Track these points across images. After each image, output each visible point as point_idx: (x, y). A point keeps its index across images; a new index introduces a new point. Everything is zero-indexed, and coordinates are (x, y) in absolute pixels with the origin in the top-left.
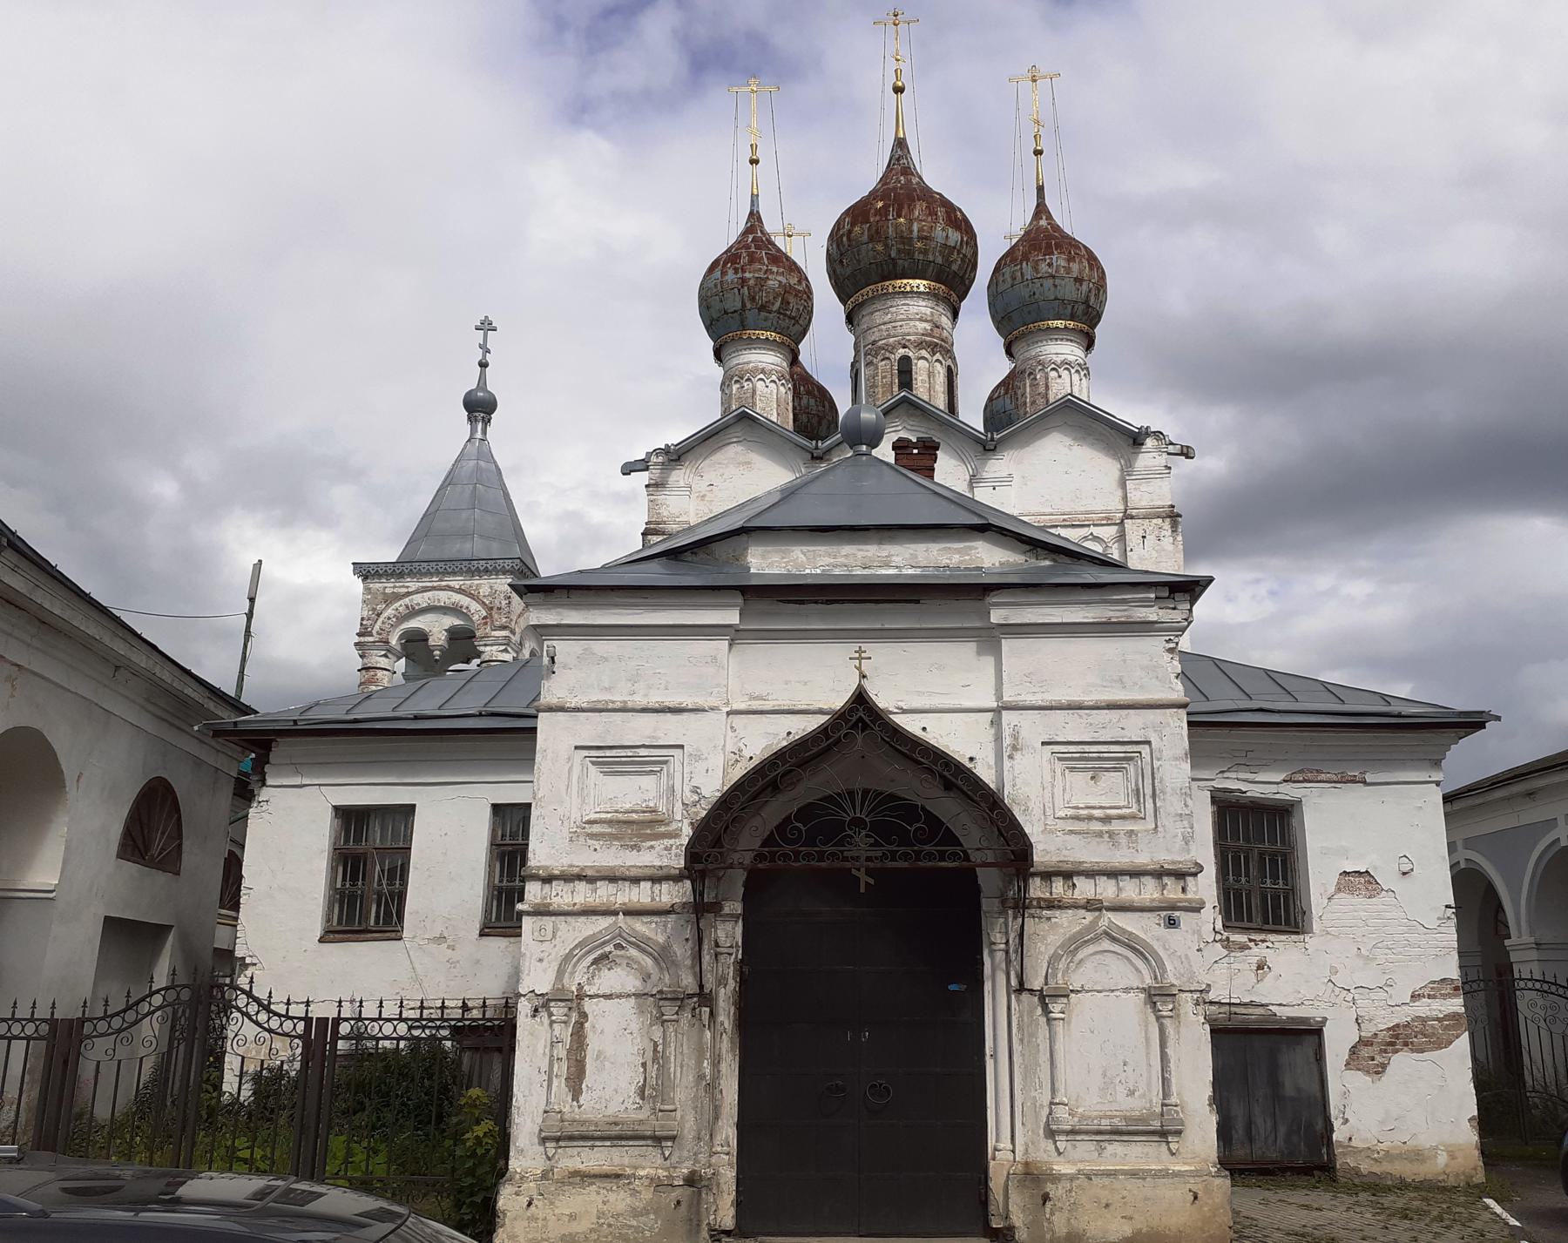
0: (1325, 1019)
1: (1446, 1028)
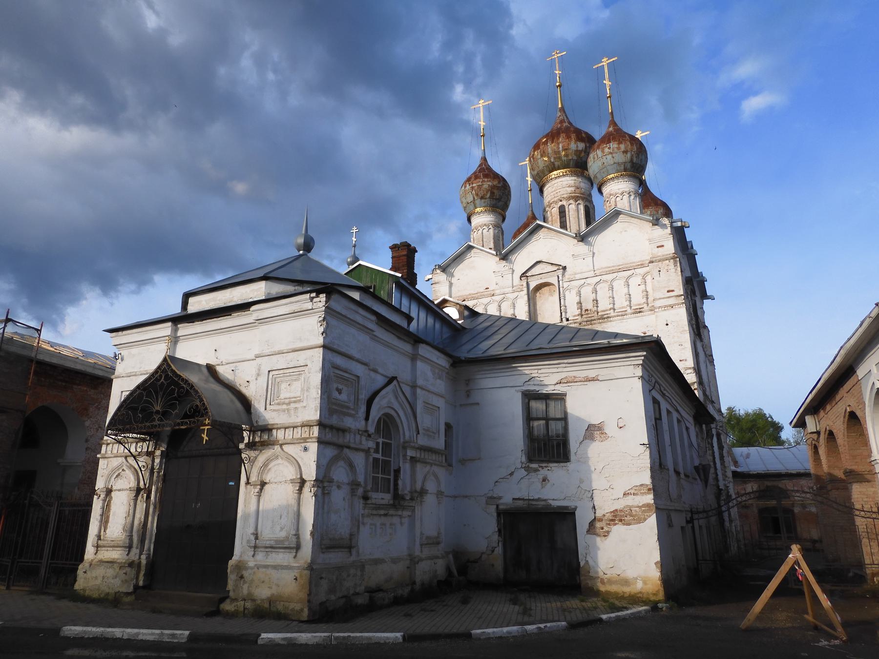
0: (576, 508)
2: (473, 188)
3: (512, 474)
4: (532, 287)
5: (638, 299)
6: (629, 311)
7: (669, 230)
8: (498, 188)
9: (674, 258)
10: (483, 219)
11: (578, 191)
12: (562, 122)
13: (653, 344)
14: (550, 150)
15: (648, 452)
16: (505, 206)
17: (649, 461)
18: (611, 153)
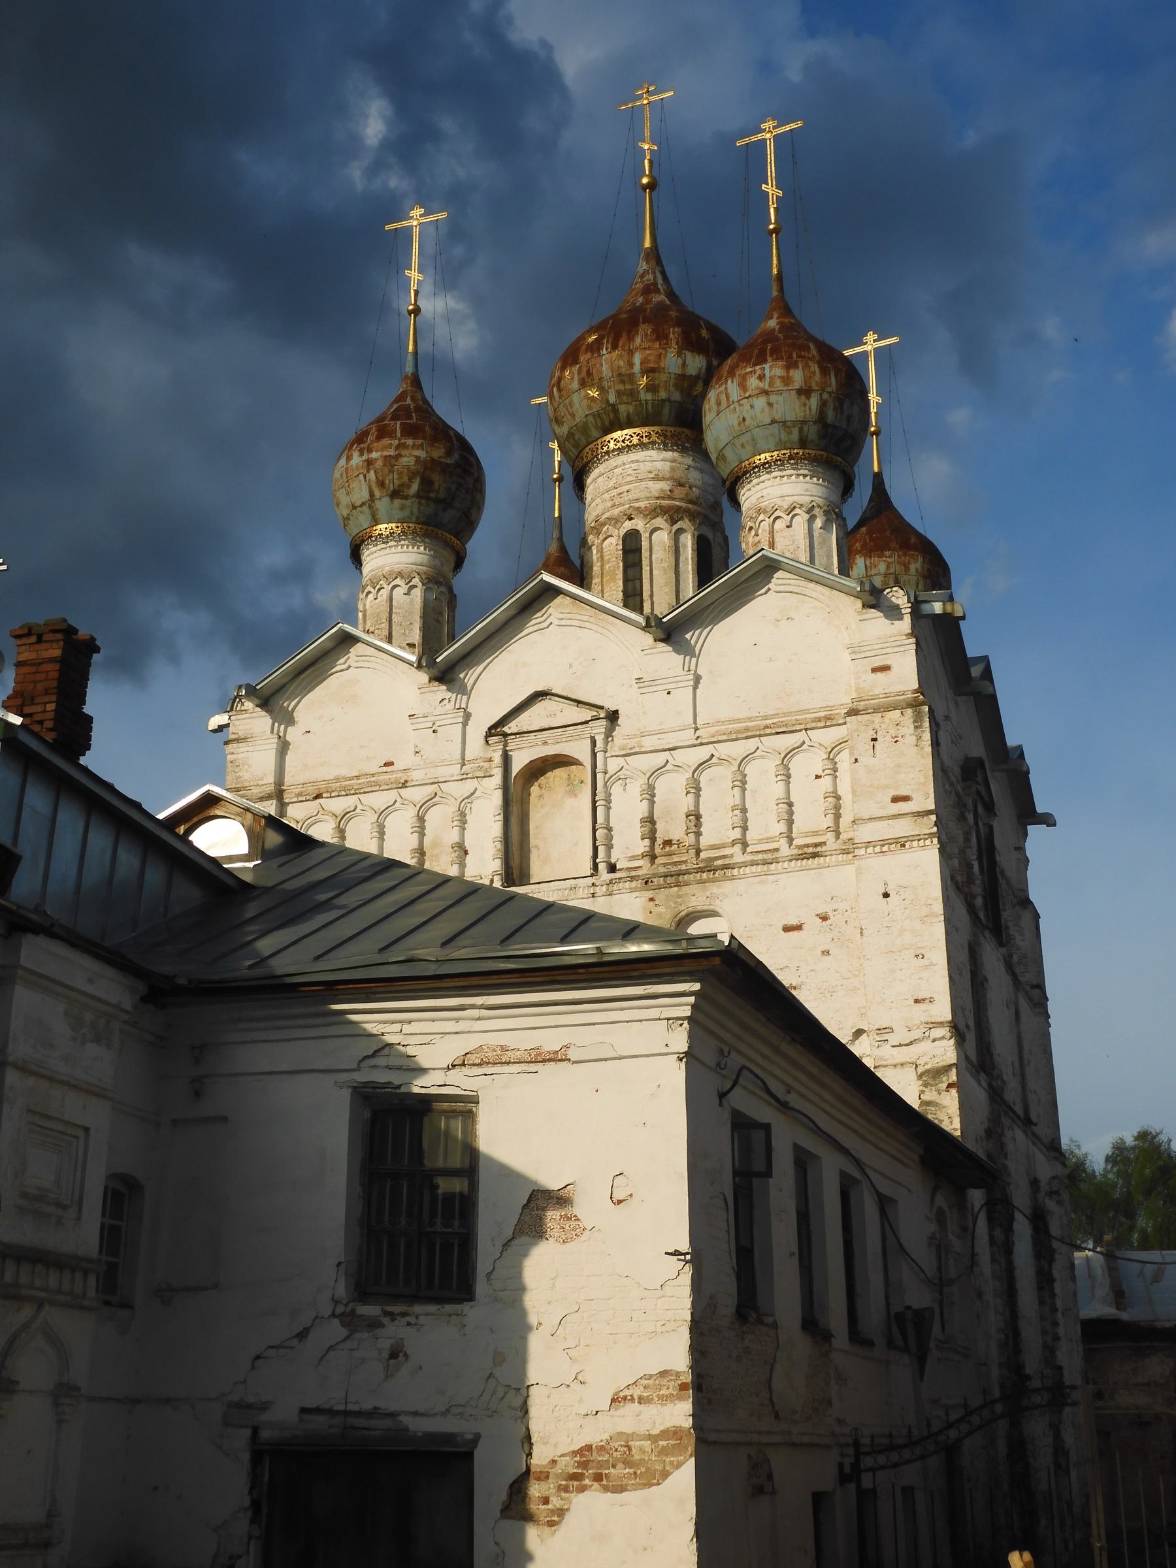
0: (477, 1438)
1: (664, 1451)
2: (369, 463)
3: (303, 1335)
4: (517, 767)
5: (811, 818)
6: (831, 843)
7: (905, 624)
8: (444, 469)
9: (914, 705)
10: (394, 559)
11: (680, 492)
12: (649, 290)
13: (717, 961)
14: (606, 370)
15: (688, 1271)
16: (466, 524)
17: (688, 1303)
18: (765, 392)
